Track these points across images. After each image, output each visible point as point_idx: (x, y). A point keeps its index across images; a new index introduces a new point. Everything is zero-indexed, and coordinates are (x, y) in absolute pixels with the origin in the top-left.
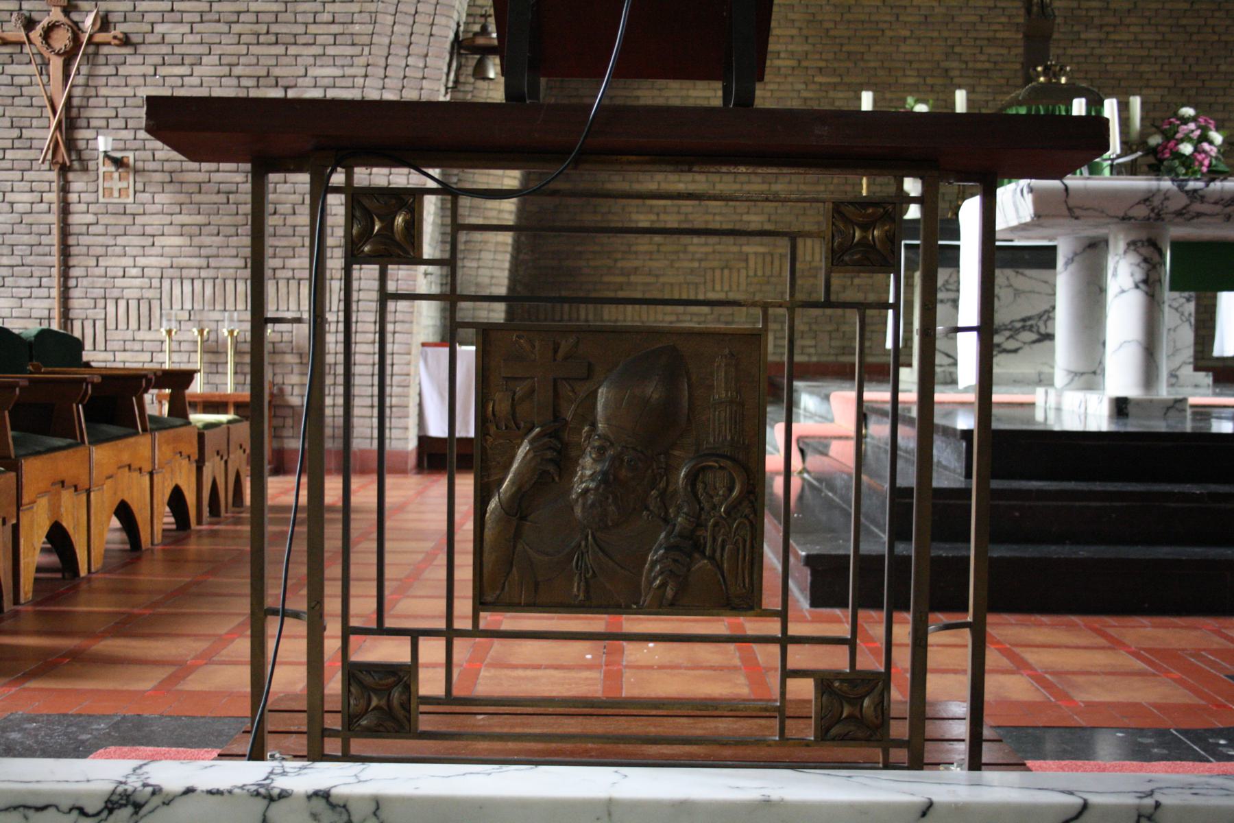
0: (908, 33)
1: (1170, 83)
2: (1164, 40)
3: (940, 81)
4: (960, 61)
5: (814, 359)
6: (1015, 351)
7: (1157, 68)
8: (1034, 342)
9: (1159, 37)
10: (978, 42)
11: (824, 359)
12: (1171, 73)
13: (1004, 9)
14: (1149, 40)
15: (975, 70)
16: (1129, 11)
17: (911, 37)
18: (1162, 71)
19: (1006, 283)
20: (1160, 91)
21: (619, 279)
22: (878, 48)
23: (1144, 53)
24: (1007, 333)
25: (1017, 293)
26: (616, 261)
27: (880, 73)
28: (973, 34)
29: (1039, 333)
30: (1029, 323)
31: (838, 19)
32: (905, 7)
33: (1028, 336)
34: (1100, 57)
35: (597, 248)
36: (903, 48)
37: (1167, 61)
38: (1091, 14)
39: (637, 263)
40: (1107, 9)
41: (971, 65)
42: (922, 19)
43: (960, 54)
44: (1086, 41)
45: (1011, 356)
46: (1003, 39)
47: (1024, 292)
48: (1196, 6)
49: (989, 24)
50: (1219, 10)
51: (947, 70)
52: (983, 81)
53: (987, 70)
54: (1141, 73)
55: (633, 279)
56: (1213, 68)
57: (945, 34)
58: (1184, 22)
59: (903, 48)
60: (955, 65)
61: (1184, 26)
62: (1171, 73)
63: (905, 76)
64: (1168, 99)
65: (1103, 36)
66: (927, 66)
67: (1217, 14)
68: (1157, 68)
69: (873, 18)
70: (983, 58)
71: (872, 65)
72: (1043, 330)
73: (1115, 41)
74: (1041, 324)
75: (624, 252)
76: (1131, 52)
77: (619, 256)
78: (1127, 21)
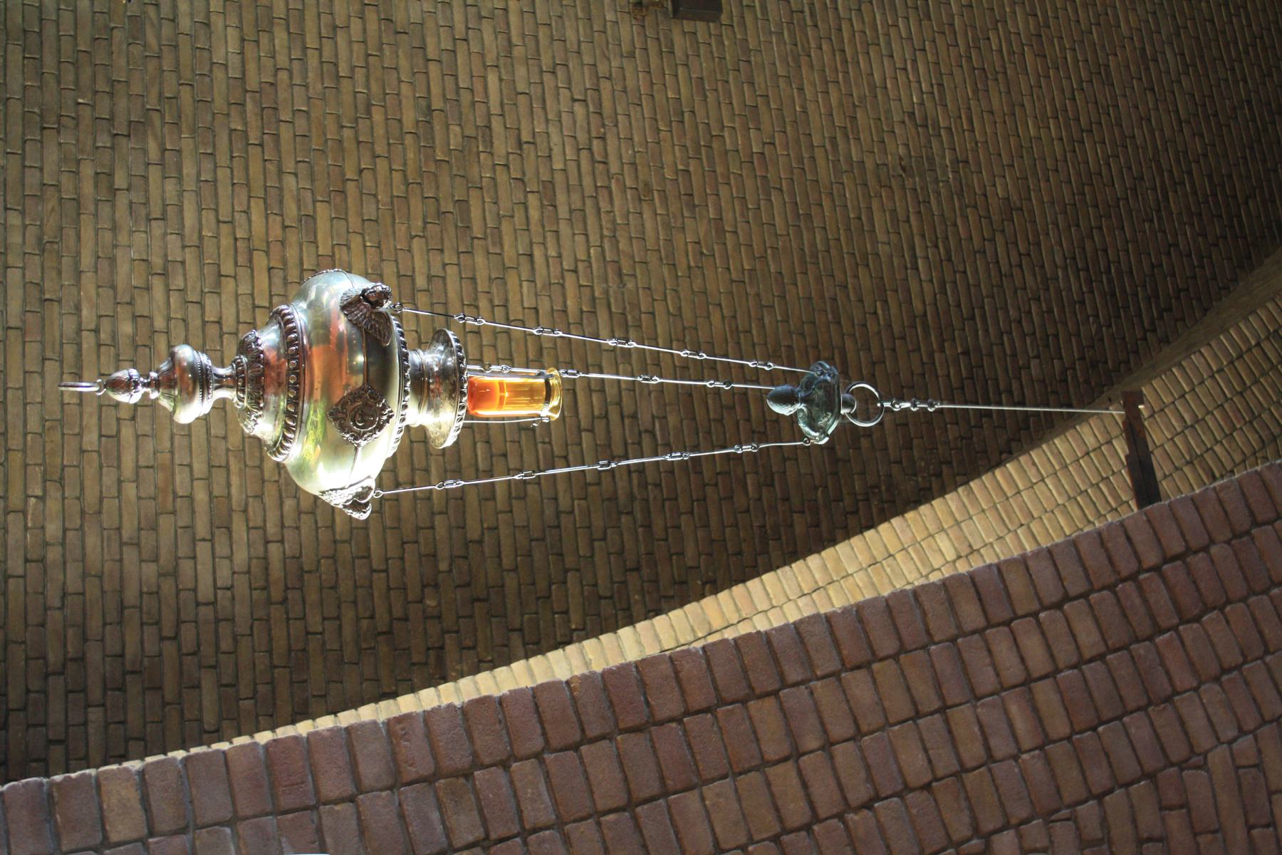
20: (234, 61)
23: (311, 42)
56: (289, 165)
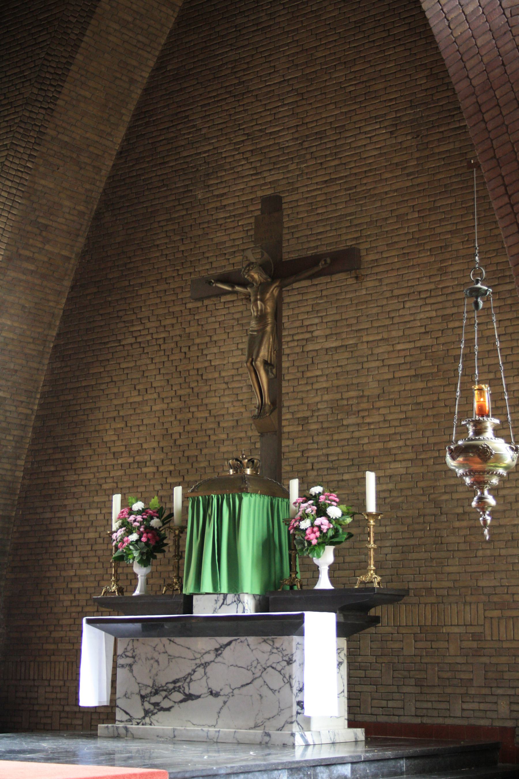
0: (224, 436)
1: (412, 456)
6: (168, 709)
16: (379, 396)
17: (227, 439)
19: (163, 650)
20: (404, 464)
21: (53, 647)
24: (164, 694)
25: (171, 658)
26: (51, 632)
27: (208, 470)
29: (185, 694)
30: (178, 685)
31: (181, 431)
33: (177, 696)
34: (359, 438)
35: (41, 622)
36: (223, 449)
38: (350, 402)
39: (62, 634)
42: (235, 424)
44: (348, 426)
45: (166, 713)
47: (175, 657)
55: (61, 646)
64: (410, 471)
65: (360, 421)
68: (402, 443)
69: (204, 427)
71: (202, 465)
72: (187, 692)
73: (369, 424)
74: (186, 685)
75: (55, 626)
76: (381, 432)
77: (52, 628)
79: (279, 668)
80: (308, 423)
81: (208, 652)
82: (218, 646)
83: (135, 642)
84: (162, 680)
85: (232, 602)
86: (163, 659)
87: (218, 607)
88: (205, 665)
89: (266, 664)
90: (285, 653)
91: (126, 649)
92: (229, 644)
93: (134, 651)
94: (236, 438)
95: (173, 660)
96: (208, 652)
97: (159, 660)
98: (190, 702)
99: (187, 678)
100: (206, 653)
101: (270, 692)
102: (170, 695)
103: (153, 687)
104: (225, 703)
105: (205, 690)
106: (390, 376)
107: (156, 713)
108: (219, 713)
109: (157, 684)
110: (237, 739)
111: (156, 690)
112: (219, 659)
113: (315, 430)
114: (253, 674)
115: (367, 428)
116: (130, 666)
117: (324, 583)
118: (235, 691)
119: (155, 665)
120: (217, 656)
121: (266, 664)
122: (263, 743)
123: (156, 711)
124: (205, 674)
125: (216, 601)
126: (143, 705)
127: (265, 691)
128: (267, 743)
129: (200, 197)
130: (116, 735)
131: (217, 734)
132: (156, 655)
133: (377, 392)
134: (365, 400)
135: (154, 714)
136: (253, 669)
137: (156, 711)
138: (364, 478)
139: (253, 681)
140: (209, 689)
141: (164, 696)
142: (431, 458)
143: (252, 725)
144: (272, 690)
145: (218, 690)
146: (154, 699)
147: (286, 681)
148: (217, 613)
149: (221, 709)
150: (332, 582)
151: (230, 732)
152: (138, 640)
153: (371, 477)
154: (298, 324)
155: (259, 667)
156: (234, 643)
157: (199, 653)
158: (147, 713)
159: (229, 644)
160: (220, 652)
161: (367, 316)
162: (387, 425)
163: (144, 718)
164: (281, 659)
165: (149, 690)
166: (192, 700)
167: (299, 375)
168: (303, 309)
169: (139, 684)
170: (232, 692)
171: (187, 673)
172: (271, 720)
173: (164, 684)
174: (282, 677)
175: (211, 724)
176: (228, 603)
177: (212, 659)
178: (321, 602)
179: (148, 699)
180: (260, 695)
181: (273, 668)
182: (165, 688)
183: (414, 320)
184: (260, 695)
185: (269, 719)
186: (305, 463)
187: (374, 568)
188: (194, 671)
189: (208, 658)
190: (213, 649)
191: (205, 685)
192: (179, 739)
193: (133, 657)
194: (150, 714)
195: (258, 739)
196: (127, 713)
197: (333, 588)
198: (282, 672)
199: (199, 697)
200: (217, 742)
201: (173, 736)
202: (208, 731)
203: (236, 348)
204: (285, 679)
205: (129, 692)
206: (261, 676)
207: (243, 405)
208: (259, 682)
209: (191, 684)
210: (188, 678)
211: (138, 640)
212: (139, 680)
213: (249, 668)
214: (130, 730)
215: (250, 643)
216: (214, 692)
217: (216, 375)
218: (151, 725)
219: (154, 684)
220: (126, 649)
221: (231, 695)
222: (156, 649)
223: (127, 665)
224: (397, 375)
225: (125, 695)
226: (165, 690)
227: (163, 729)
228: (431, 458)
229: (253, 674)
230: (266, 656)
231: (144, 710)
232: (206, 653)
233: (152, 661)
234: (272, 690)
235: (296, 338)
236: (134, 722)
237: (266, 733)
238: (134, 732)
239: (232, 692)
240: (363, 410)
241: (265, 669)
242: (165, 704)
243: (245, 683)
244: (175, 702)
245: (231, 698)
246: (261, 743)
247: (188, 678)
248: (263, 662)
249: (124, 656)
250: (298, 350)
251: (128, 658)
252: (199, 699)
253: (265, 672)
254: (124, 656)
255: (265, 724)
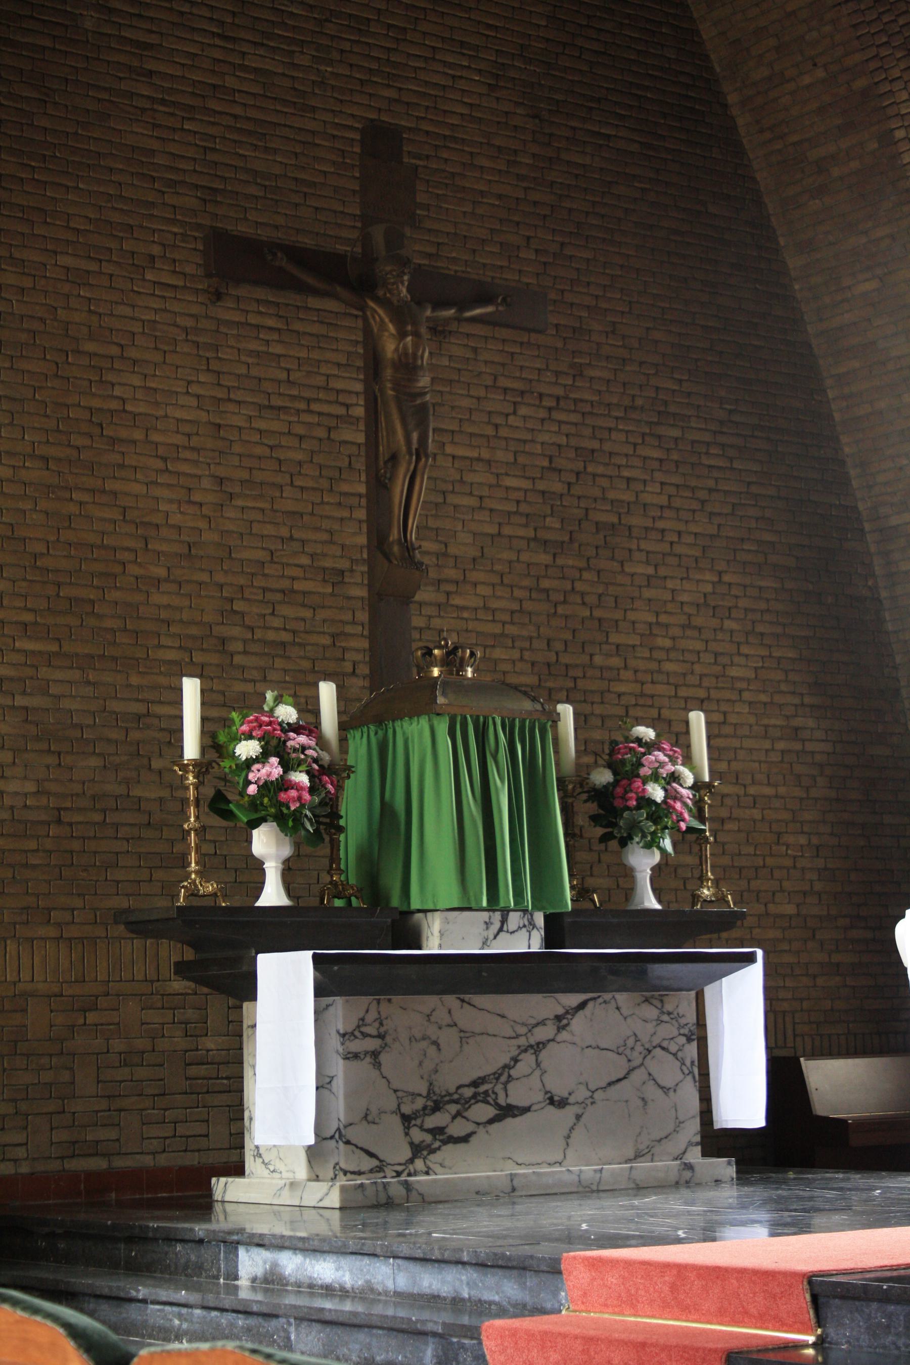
0: (162, 572)
2: (521, 611)
3: (214, 659)
4: (244, 625)
5: (24, 1169)
6: (465, 1139)
7: (516, 654)
8: (491, 1121)
9: (515, 606)
10: (269, 596)
11: (40, 1167)
12: (533, 664)
13: (303, 542)
14: (502, 610)
15: (265, 642)
17: (167, 580)
18: (522, 659)
19: (447, 1020)
22: (116, 595)
23: (497, 629)
25: (465, 1036)
28: (259, 582)
29: (497, 1105)
32: (157, 526)
33: (482, 1111)
36: (156, 598)
37: (526, 644)
40: (445, 555)
41: (259, 634)
43: (243, 614)
45: (461, 1146)
46: (304, 593)
47: (474, 1034)
48: (560, 561)
49: (284, 565)
50: (588, 568)
51: (223, 641)
52: (279, 663)
53: (283, 644)
54: (496, 662)
56: (585, 659)
57: (220, 578)
58: (545, 584)
59: (156, 598)
60: (236, 631)
61: (547, 591)
62: (533, 664)
63: (159, 646)
65: (442, 598)
66: (194, 631)
67: (586, 575)
70: (277, 622)
71: (109, 623)
72: (502, 1101)
74: (499, 1088)
78: (473, 576)
79: (673, 1048)
80: (342, 582)
81: (542, 1023)
82: (560, 1011)
83: (384, 1007)
84: (448, 1081)
85: (520, 928)
86: (449, 1038)
87: (491, 937)
88: (538, 1048)
89: (650, 1041)
90: (683, 1021)
91: (363, 1019)
92: (582, 1006)
93: (381, 1024)
94: (188, 581)
95: (471, 1041)
96: (542, 1023)
97: (441, 1041)
98: (509, 1121)
99: (500, 1075)
100: (537, 1025)
101: (660, 1091)
102: (467, 1109)
103: (428, 1097)
104: (578, 1117)
105: (540, 1096)
106: (493, 530)
107: (439, 1148)
108: (569, 1137)
109: (437, 1090)
110: (634, 1181)
111: (435, 1102)
112: (564, 1035)
113: (358, 598)
114: (629, 1061)
115: (455, 615)
116: (375, 1054)
117: (272, 895)
118: (596, 1095)
119: (432, 1050)
120: (560, 1029)
121: (650, 1041)
122: (682, 1181)
123: (437, 1144)
124: (538, 1064)
125: (488, 924)
126: (407, 1134)
127: (652, 1092)
128: (687, 1182)
129: (88, 25)
130: (383, 1200)
131: (598, 1175)
132: (432, 1031)
133: (473, 552)
134: (451, 562)
135: (433, 1151)
136: (628, 1052)
137: (437, 1144)
138: (687, 723)
139: (628, 1073)
140: (546, 1093)
141: (454, 1112)
142: (561, 689)
143: (631, 1154)
144: (662, 1088)
145: (566, 1095)
146: (432, 1122)
147: (687, 1072)
148: (489, 947)
149: (572, 1129)
150: (660, 901)
151: (622, 1169)
152: (389, 1000)
153: (191, 688)
154: (320, 381)
155: (639, 1048)
156: (590, 1005)
157: (524, 1024)
158: (417, 1150)
159: (582, 1006)
160: (565, 1022)
161: (453, 407)
162: (490, 618)
163: (411, 1161)
164: (676, 1033)
165: (420, 1103)
166: (514, 1116)
167: (325, 484)
168: (329, 356)
169: (395, 1091)
170: (592, 1097)
171: (501, 1064)
172: (664, 1141)
173: (452, 1089)
174: (678, 1064)
175: (552, 1160)
176: (511, 930)
177: (551, 1037)
178: (280, 931)
179: (418, 1122)
180: (643, 1099)
181: (663, 1049)
182: (456, 1097)
183: (532, 441)
184: (643, 1099)
185: (660, 1141)
186: (339, 659)
187: (712, 877)
188: (516, 1060)
189: (541, 1034)
190: (552, 1017)
191: (540, 1085)
192: (524, 1193)
193: (381, 1036)
194: (425, 1153)
195: (673, 1176)
196: (371, 1155)
197: (658, 906)
198: (680, 1054)
199: (527, 1110)
200: (598, 1191)
201: (509, 1189)
202: (581, 1171)
203: (185, 390)
204: (684, 1068)
205: (374, 1110)
206: (642, 1064)
207: (204, 516)
208: (638, 1076)
209: (509, 1086)
210: (504, 1074)
211: (389, 1000)
212: (396, 1084)
213: (620, 1050)
214: (416, 1186)
215: (620, 1004)
216: (556, 1098)
217: (138, 435)
218: (427, 1173)
219: (430, 1091)
220: (363, 1019)
221: (589, 1101)
222: (433, 1019)
223: (366, 1053)
224: (507, 530)
225: (366, 1117)
226: (456, 1102)
227: (488, 1177)
228: (561, 689)
229: (629, 1061)
230: (650, 1027)
231: (411, 1144)
232: (537, 1025)
233: (424, 1044)
234: (662, 1088)
235: (315, 407)
236: (389, 1172)
237: (685, 1164)
238: (421, 1189)
239: (592, 1097)
240: (447, 581)
241: (649, 1051)
242: (458, 1129)
243: (614, 1079)
244: (478, 1124)
245: (590, 1107)
246: (677, 1183)
247: (504, 1074)
248: (645, 1039)
249: (357, 1033)
250: (321, 433)
251: (368, 1039)
252: (529, 1114)
253: (649, 1057)
254: (357, 1033)
255: (654, 1150)
